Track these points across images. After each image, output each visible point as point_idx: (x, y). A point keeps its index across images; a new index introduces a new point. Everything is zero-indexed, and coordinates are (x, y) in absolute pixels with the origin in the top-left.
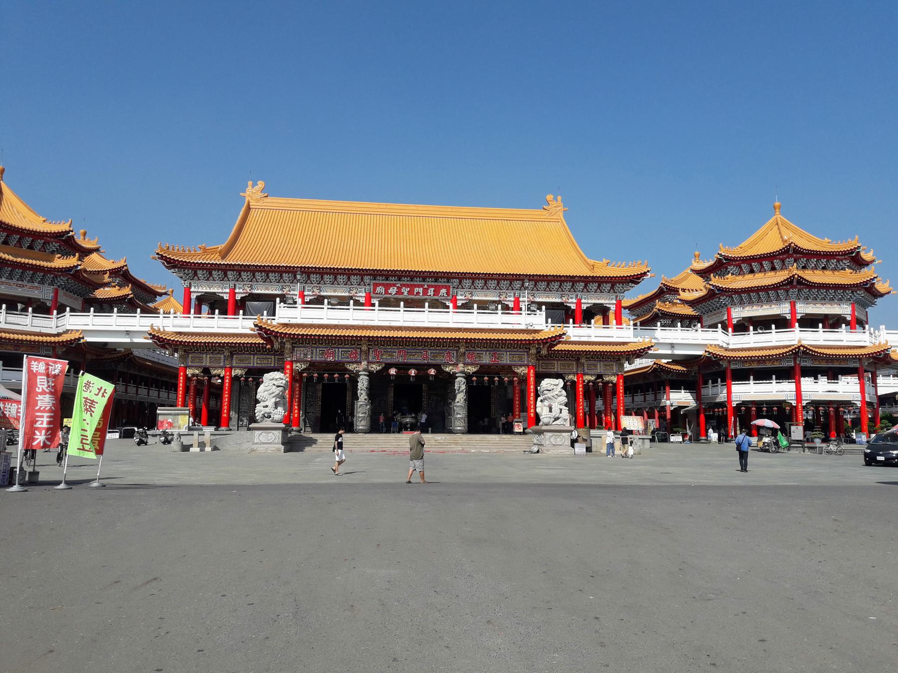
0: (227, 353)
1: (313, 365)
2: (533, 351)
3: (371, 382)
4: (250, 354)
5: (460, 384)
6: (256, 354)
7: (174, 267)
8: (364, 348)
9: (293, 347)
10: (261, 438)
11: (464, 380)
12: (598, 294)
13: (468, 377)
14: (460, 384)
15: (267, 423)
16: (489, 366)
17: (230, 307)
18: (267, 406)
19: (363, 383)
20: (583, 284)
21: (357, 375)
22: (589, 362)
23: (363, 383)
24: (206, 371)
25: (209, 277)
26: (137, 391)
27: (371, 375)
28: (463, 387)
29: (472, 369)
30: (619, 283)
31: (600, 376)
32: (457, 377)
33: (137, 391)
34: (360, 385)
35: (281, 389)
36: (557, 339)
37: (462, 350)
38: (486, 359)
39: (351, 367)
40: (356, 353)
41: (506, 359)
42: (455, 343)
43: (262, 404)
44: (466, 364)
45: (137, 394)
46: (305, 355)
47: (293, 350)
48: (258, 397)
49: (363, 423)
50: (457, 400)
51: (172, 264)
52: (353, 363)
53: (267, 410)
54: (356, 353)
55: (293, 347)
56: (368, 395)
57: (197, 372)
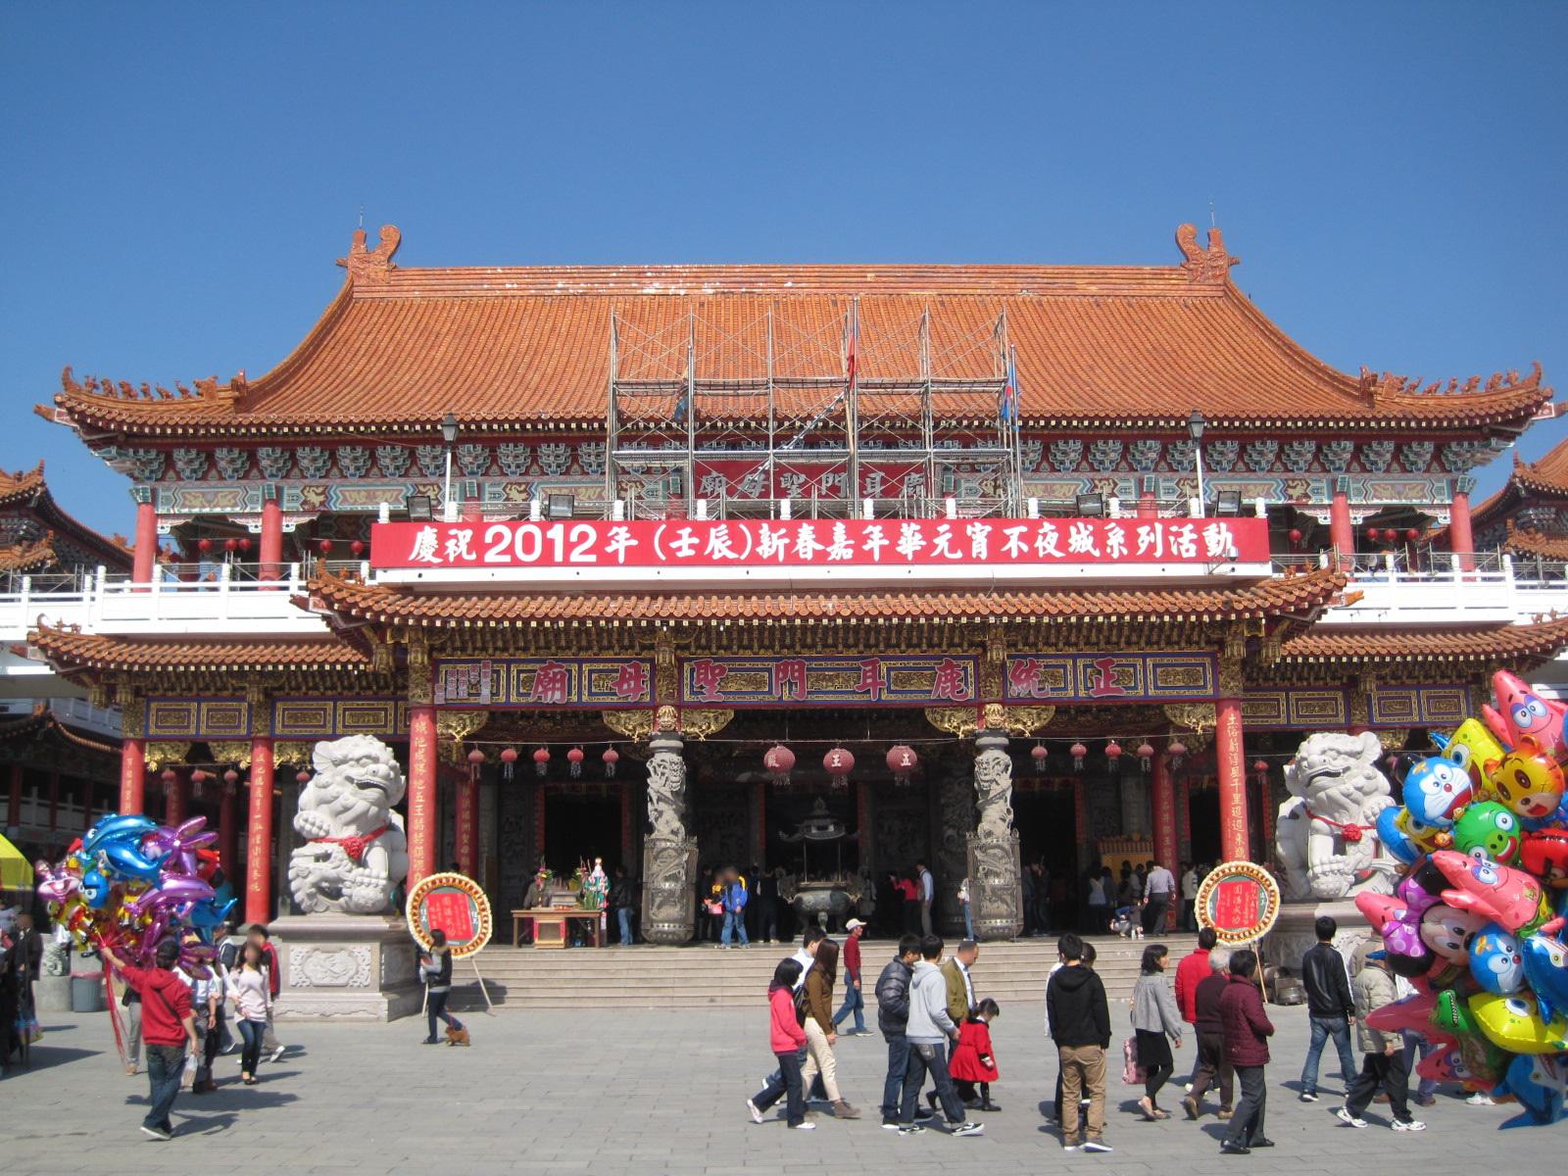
0: (254, 696)
1: (500, 722)
2: (1237, 650)
3: (691, 777)
4: (323, 698)
5: (994, 771)
6: (341, 697)
7: (107, 442)
8: (664, 657)
9: (435, 664)
10: (309, 968)
11: (1005, 758)
12: (1397, 478)
13: (1017, 748)
14: (994, 771)
15: (327, 918)
16: (1083, 708)
17: (268, 556)
18: (326, 857)
19: (665, 775)
20: (1349, 445)
21: (644, 751)
22: (1384, 693)
23: (665, 775)
24: (199, 751)
25: (207, 468)
26: (53, 817)
27: (690, 751)
28: (1005, 781)
29: (1029, 723)
30: (1460, 440)
31: (199, 751)
32: (980, 750)
33: (53, 817)
34: (656, 785)
35: (373, 794)
36: (1298, 619)
37: (997, 654)
38: (1079, 683)
39: (629, 725)
40: (637, 677)
41: (1143, 681)
42: (971, 636)
43: (312, 848)
44: (1011, 704)
45: (53, 825)
46: (475, 688)
47: (436, 672)
48: (298, 822)
49: (674, 911)
50: (983, 826)
51: (101, 434)
52: (627, 708)
53: (326, 869)
54: (637, 677)
55: (435, 664)
56: (683, 818)
57: (174, 757)
